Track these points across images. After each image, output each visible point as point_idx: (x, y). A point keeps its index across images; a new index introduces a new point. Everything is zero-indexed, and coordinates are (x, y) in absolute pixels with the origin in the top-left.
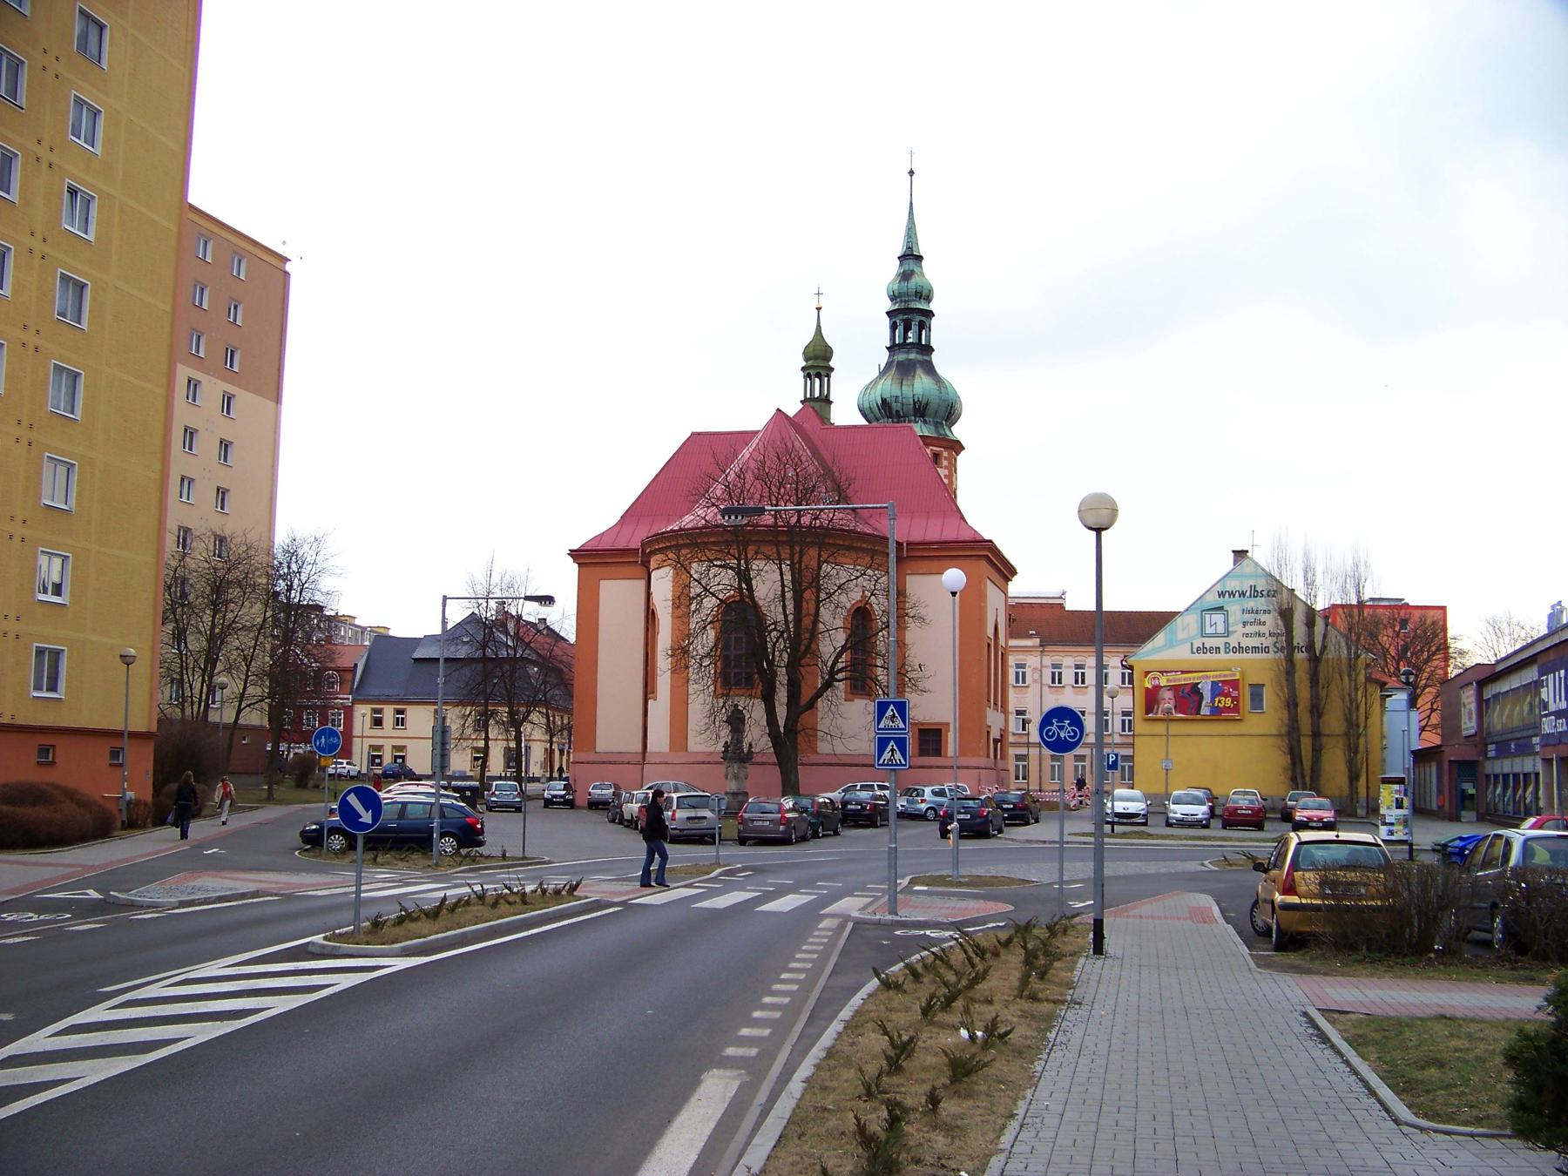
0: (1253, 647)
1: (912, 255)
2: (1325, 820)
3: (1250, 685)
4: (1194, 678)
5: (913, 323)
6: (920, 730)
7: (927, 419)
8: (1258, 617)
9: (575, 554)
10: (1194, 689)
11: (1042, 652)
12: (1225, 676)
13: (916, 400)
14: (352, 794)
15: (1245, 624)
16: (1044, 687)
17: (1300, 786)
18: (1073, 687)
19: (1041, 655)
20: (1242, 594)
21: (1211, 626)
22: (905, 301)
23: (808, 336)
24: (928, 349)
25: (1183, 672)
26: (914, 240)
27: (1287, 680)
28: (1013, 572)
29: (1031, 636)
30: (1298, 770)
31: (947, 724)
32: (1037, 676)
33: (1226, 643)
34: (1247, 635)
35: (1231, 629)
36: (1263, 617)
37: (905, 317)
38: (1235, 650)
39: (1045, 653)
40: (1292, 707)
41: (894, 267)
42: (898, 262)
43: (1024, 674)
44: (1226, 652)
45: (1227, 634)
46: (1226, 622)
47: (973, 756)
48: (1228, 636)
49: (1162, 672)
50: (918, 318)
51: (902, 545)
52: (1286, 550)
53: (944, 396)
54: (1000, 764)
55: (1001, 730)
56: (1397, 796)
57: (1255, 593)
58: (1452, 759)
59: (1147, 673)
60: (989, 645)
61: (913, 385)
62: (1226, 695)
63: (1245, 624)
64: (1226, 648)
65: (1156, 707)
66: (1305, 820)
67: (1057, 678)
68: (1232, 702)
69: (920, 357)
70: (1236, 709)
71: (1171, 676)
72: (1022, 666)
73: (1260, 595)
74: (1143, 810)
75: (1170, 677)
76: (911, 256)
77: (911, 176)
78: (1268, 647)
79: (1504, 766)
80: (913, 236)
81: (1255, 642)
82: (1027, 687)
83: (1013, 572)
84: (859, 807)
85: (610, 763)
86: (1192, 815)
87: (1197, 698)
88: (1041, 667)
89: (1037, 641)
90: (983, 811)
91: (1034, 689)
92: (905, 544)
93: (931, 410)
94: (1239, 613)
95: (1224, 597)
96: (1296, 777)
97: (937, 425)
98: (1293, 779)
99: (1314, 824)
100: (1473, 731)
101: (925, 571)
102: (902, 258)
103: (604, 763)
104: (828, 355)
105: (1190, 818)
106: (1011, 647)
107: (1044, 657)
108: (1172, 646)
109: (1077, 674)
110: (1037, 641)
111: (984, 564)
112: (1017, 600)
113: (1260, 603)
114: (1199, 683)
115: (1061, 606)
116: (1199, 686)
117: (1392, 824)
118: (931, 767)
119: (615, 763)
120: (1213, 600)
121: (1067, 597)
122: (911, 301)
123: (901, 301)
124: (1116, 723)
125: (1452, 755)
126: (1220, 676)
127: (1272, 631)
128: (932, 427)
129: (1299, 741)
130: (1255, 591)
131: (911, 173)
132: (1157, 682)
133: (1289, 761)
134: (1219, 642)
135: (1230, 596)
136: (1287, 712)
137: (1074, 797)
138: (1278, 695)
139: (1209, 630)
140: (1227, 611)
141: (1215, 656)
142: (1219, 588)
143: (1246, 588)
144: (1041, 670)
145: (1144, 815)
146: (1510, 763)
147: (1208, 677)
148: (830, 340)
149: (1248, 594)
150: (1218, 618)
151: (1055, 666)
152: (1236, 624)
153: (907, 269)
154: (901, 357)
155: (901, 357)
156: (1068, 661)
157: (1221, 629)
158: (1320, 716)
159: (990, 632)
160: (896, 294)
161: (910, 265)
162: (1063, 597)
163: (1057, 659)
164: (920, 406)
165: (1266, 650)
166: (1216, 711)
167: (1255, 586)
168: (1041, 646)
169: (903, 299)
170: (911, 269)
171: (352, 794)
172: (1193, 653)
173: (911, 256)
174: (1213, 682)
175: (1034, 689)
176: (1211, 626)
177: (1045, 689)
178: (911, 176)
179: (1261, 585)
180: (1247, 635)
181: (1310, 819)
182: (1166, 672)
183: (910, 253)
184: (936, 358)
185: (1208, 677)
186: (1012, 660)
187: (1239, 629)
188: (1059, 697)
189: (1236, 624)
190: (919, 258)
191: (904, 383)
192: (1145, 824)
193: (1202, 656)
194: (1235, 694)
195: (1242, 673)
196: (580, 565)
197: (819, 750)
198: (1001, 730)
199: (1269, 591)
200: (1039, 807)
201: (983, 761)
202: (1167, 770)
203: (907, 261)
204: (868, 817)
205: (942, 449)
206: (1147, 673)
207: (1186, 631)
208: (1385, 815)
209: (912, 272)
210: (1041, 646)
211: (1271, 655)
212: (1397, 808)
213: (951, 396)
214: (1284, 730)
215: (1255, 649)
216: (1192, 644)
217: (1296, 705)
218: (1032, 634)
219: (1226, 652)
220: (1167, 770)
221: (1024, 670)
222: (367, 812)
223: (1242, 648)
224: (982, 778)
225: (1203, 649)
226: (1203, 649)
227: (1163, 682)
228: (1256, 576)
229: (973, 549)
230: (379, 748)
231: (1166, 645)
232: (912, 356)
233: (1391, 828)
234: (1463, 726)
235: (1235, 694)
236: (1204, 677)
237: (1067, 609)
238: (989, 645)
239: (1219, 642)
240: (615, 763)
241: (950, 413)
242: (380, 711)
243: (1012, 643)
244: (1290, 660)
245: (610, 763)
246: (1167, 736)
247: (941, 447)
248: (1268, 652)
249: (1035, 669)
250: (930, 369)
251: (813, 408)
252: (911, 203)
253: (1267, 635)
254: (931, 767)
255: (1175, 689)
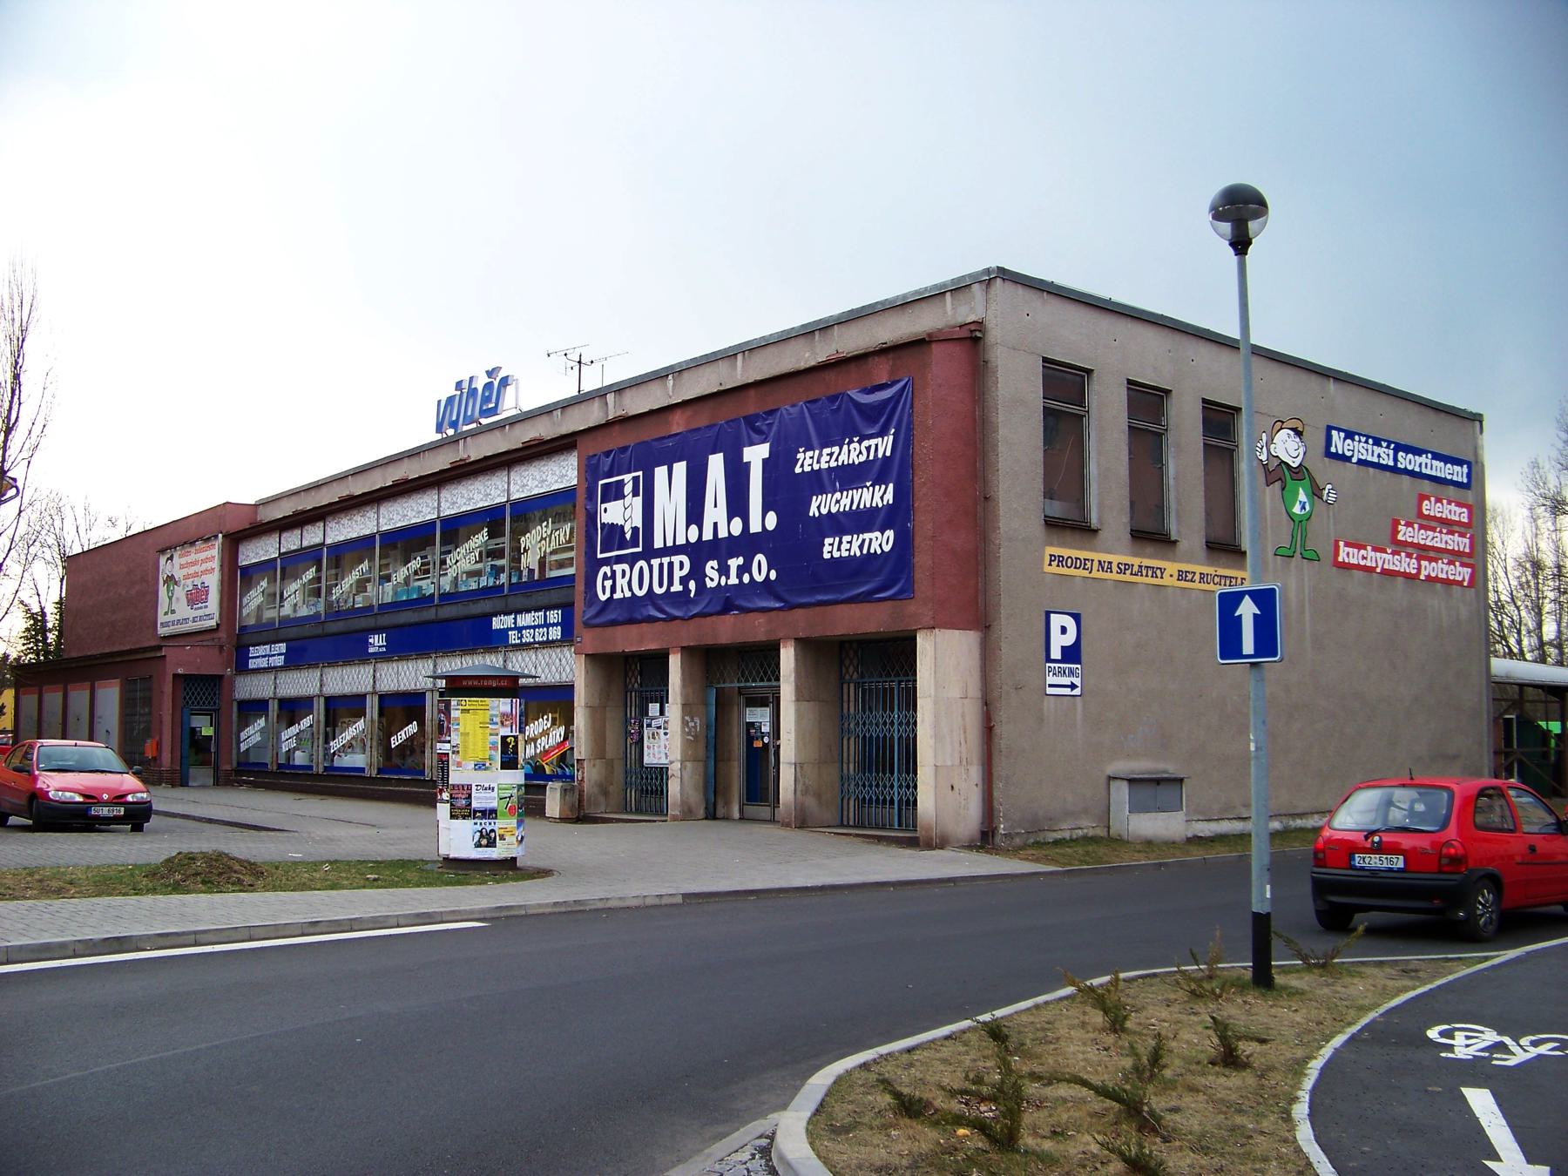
2: (130, 798)
14: (1244, 653)
56: (505, 731)
58: (180, 671)
66: (79, 799)
79: (431, 667)
99: (104, 811)
100: (213, 623)
117: (490, 813)
125: (181, 666)
146: (60, 695)
158: (505, 386)
171: (1244, 653)
181: (91, 797)
208: (469, 787)
212: (504, 767)
222: (1241, 615)
233: (487, 825)
234: (161, 618)
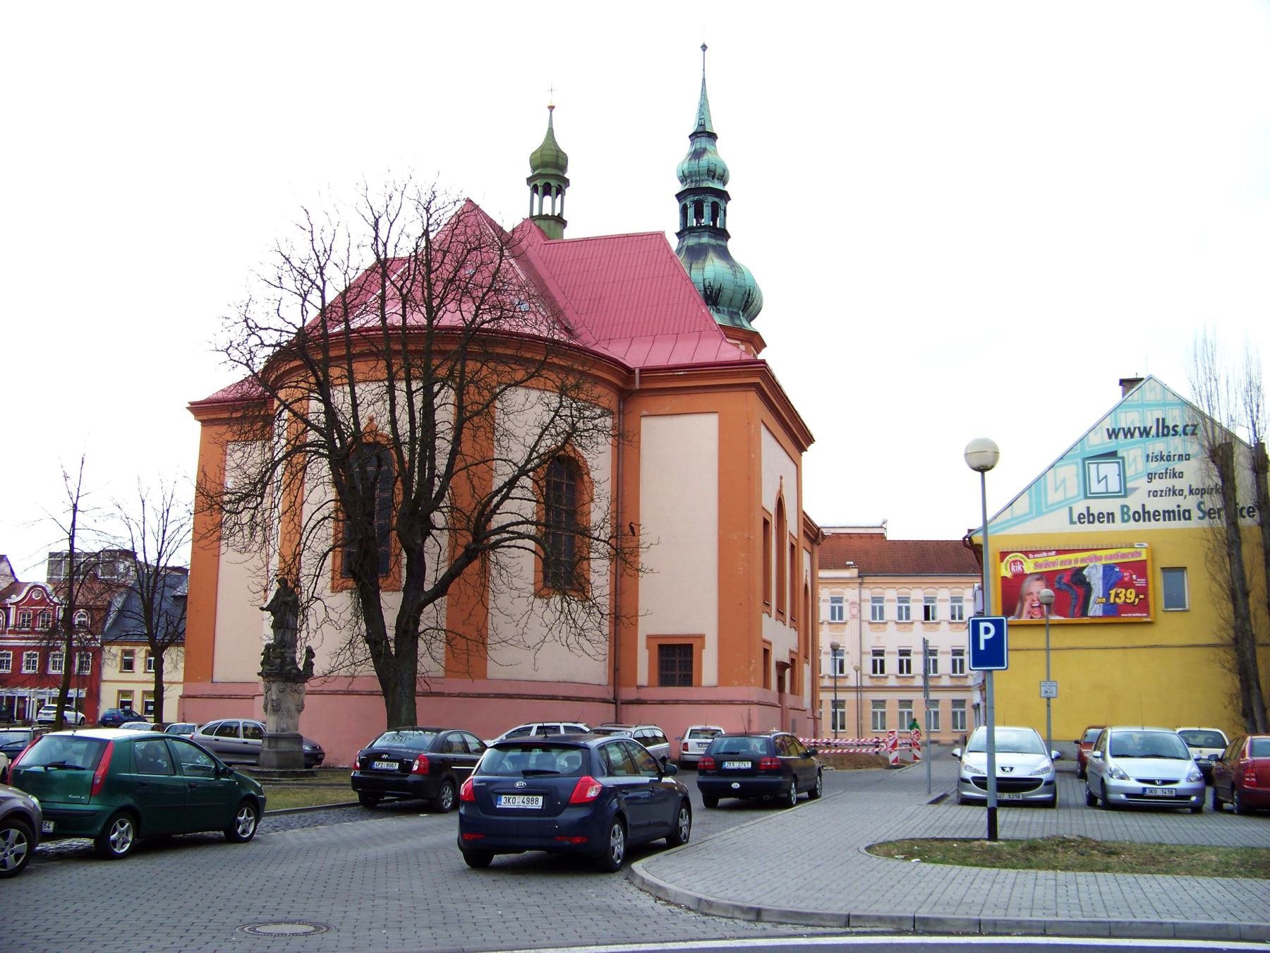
0: (1164, 512)
1: (704, 132)
3: (1162, 568)
4: (1076, 561)
5: (705, 204)
6: (661, 646)
7: (721, 308)
8: (1171, 465)
9: (200, 409)
10: (1077, 578)
11: (861, 584)
12: (1124, 556)
13: (707, 284)
15: (1151, 477)
16: (863, 624)
17: (1259, 725)
18: (897, 623)
19: (860, 588)
20: (1145, 432)
21: (1099, 482)
22: (696, 181)
23: (537, 141)
24: (723, 234)
25: (1059, 552)
26: (707, 118)
27: (1229, 555)
28: (810, 440)
29: (848, 567)
30: (1255, 700)
31: (702, 637)
32: (855, 611)
33: (1123, 507)
34: (1155, 493)
35: (1129, 485)
36: (1179, 466)
37: (696, 198)
38: (1138, 516)
39: (864, 586)
40: (1239, 596)
41: (686, 147)
42: (689, 142)
43: (841, 609)
44: (1124, 521)
45: (1125, 492)
46: (1123, 476)
47: (740, 685)
48: (1125, 496)
49: (1026, 553)
50: (711, 199)
51: (634, 371)
52: (1215, 370)
53: (740, 281)
54: (790, 700)
55: (791, 652)
57: (1164, 430)
59: (1004, 555)
60: (766, 523)
61: (703, 268)
62: (1127, 586)
63: (1151, 477)
64: (1123, 513)
65: (1019, 606)
67: (878, 613)
68: (1137, 596)
69: (713, 241)
70: (1143, 606)
71: (1041, 559)
72: (839, 600)
73: (1172, 432)
74: (1046, 769)
75: (1040, 561)
76: (703, 134)
77: (704, 50)
78: (1189, 511)
80: (706, 113)
81: (1168, 503)
82: (845, 623)
83: (810, 440)
84: (396, 766)
85: (230, 697)
86: (1165, 782)
87: (1082, 591)
88: (860, 600)
89: (854, 572)
90: (589, 785)
91: (853, 626)
92: (637, 371)
93: (725, 297)
94: (1141, 461)
95: (1116, 437)
96: (1252, 710)
97: (733, 315)
98: (1247, 713)
101: (666, 410)
102: (694, 136)
103: (221, 697)
104: (561, 161)
105: (1159, 790)
106: (821, 578)
107: (863, 591)
108: (1040, 513)
109: (900, 608)
110: (854, 572)
111: (753, 396)
112: (833, 531)
113: (1175, 445)
114: (1084, 568)
115: (882, 536)
116: (1085, 572)
118: (676, 702)
119: (236, 697)
120: (1100, 442)
121: (888, 526)
122: (702, 181)
123: (692, 182)
124: (945, 663)
126: (1117, 556)
127: (1194, 487)
128: (727, 317)
129: (1254, 651)
130: (1164, 427)
131: (704, 47)
132: (1019, 568)
133: (1238, 684)
134: (1113, 505)
135: (1126, 436)
136: (1230, 606)
137: (894, 745)
138: (1213, 578)
139: (1096, 487)
140: (1123, 458)
141: (1106, 527)
142: (1109, 424)
143: (1150, 422)
144: (860, 605)
145: (1049, 783)
147: (1099, 559)
148: (563, 144)
149: (1153, 431)
150: (1110, 469)
151: (875, 600)
152: (1137, 476)
153: (698, 147)
154: (691, 241)
155: (691, 241)
156: (890, 593)
157: (1114, 486)
159: (771, 507)
160: (686, 172)
161: (703, 142)
162: (884, 526)
163: (877, 592)
164: (711, 292)
165: (1186, 515)
166: (1112, 610)
167: (1163, 419)
168: (859, 577)
169: (694, 178)
170: (703, 146)
172: (1072, 522)
173: (703, 134)
174: (1105, 567)
175: (853, 626)
176: (1099, 482)
177: (865, 625)
178: (704, 50)
179: (1175, 418)
180: (1155, 493)
182: (1034, 552)
183: (702, 130)
184: (731, 245)
185: (1099, 559)
186: (824, 594)
187: (1143, 485)
188: (880, 634)
189: (1137, 476)
190: (712, 136)
191: (693, 266)
192: (1049, 804)
193: (1087, 527)
194: (1140, 582)
195: (1152, 552)
196: (204, 422)
197: (490, 674)
198: (791, 652)
199: (1185, 427)
200: (818, 765)
201: (755, 693)
202: (1049, 699)
203: (698, 139)
204: (416, 789)
205: (739, 342)
206: (1004, 555)
207: (1061, 490)
209: (704, 150)
210: (859, 577)
211: (1196, 523)
213: (748, 283)
214: (1228, 635)
215: (1169, 515)
216: (1071, 509)
217: (1246, 594)
218: (849, 565)
219: (1124, 521)
220: (1049, 699)
221: (840, 605)
223: (1148, 512)
224: (753, 718)
225: (1088, 517)
226: (1088, 517)
227: (1029, 567)
228: (1165, 405)
229: (737, 375)
230: (128, 693)
231: (1031, 512)
232: (705, 240)
235: (1140, 582)
236: (1090, 559)
237: (888, 539)
238: (766, 523)
239: (1113, 505)
240: (236, 697)
241: (747, 301)
242: (131, 653)
243: (823, 574)
244: (1233, 524)
245: (230, 697)
246: (1048, 649)
247: (737, 339)
248: (1189, 518)
249: (853, 603)
250: (724, 254)
251: (539, 227)
252: (704, 79)
253: (1186, 492)
254: (676, 702)
255: (1048, 578)
